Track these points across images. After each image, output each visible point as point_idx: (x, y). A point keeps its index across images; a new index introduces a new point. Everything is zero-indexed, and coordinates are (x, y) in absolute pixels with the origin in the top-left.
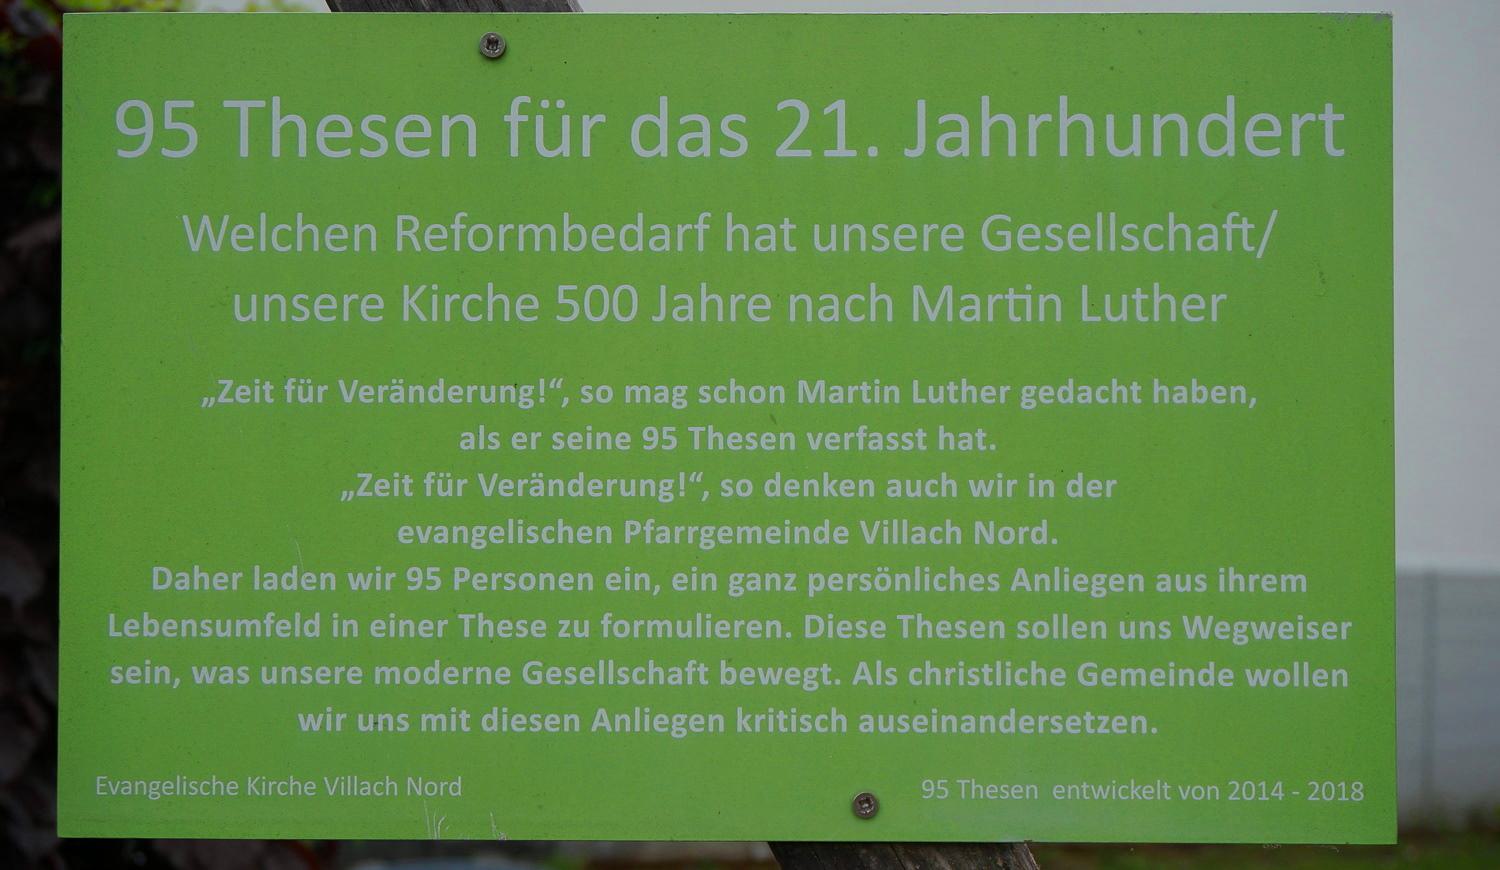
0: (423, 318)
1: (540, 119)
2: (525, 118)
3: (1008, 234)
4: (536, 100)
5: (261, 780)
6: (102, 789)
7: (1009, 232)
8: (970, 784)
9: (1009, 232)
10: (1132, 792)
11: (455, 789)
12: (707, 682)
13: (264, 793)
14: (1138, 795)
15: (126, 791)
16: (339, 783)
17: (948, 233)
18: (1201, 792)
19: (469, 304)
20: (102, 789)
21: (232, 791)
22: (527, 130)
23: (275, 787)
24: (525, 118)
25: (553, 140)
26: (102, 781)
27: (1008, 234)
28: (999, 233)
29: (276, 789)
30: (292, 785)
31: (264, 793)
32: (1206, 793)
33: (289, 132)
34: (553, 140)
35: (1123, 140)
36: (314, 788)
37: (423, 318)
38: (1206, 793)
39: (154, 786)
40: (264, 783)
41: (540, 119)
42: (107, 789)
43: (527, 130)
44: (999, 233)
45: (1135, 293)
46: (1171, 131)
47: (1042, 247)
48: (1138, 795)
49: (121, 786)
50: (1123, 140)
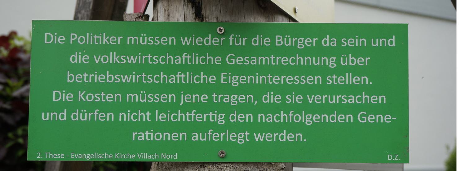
0: (118, 158)
1: (236, 39)
2: (233, 38)
3: (365, 118)
4: (235, 35)
5: (119, 154)
6: (73, 156)
7: (234, 59)
8: (49, 154)
9: (234, 59)
10: (116, 156)
11: (175, 157)
12: (249, 140)
13: (120, 158)
14: (118, 157)
15: (80, 157)
16: (142, 154)
17: (238, 59)
18: (169, 156)
19: (162, 58)
20: (73, 156)
21: (111, 157)
22: (233, 41)
23: (123, 156)
24: (233, 38)
25: (238, 42)
26: (73, 154)
27: (365, 118)
28: (363, 117)
29: (173, 157)
30: (156, 156)
31: (120, 158)
32: (170, 157)
33: (51, 156)
34: (238, 42)
35: (316, 62)
36: (112, 156)
37: (118, 158)
38: (170, 157)
39: (88, 156)
40: (120, 155)
41: (236, 39)
42: (74, 156)
43: (233, 41)
44: (363, 117)
45: (268, 76)
46: (383, 42)
47: (243, 63)
48: (118, 157)
49: (79, 156)
50: (316, 62)
